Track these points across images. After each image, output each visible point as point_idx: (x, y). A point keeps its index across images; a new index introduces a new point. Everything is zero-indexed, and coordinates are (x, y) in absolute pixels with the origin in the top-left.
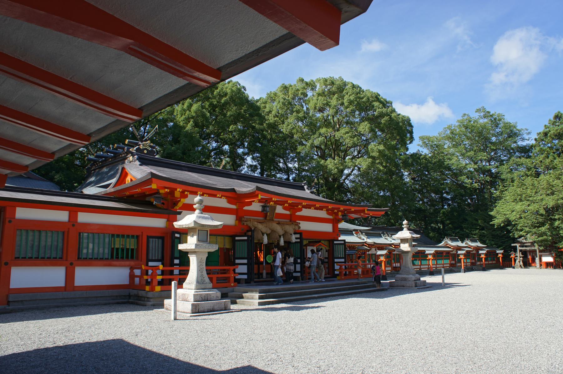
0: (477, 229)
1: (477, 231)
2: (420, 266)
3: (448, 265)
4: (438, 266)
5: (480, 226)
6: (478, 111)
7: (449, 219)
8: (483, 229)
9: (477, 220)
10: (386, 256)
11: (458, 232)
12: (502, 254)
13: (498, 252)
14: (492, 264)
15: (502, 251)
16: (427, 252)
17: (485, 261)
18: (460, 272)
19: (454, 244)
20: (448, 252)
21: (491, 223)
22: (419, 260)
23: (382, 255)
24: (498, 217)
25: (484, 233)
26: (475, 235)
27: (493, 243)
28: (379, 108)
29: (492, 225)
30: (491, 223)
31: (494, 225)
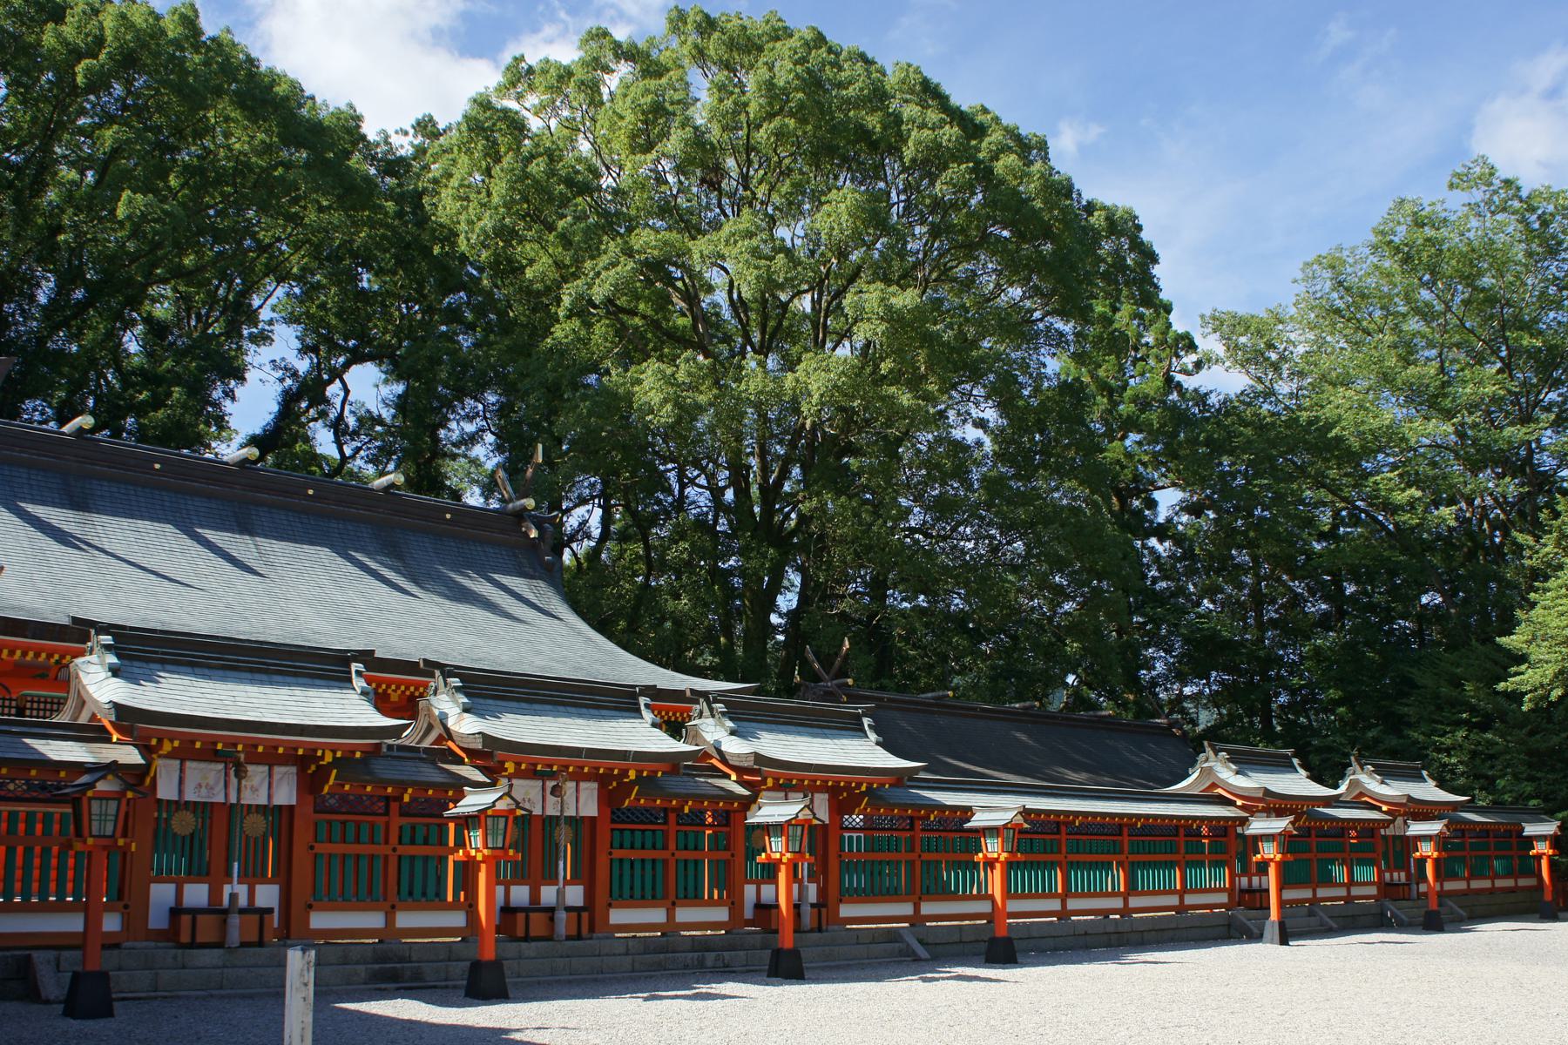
0: (1459, 724)
1: (1461, 733)
2: (1125, 897)
3: (1223, 898)
4: (1355, 891)
5: (1473, 710)
6: (1460, 181)
7: (1339, 682)
8: (1484, 726)
9: (1457, 683)
10: (1440, 841)
11: (1376, 741)
12: (1555, 841)
13: (1530, 830)
14: (1511, 890)
15: (1550, 828)
16: (979, 820)
17: (1437, 876)
18: (1255, 936)
19: (1394, 790)
20: (1368, 830)
21: (1501, 686)
22: (1343, 863)
23: (1270, 837)
24: (1536, 653)
25: (1491, 743)
26: (1448, 751)
27: (1528, 788)
28: (922, 126)
29: (1505, 694)
30: (1501, 686)
31: (1516, 697)
